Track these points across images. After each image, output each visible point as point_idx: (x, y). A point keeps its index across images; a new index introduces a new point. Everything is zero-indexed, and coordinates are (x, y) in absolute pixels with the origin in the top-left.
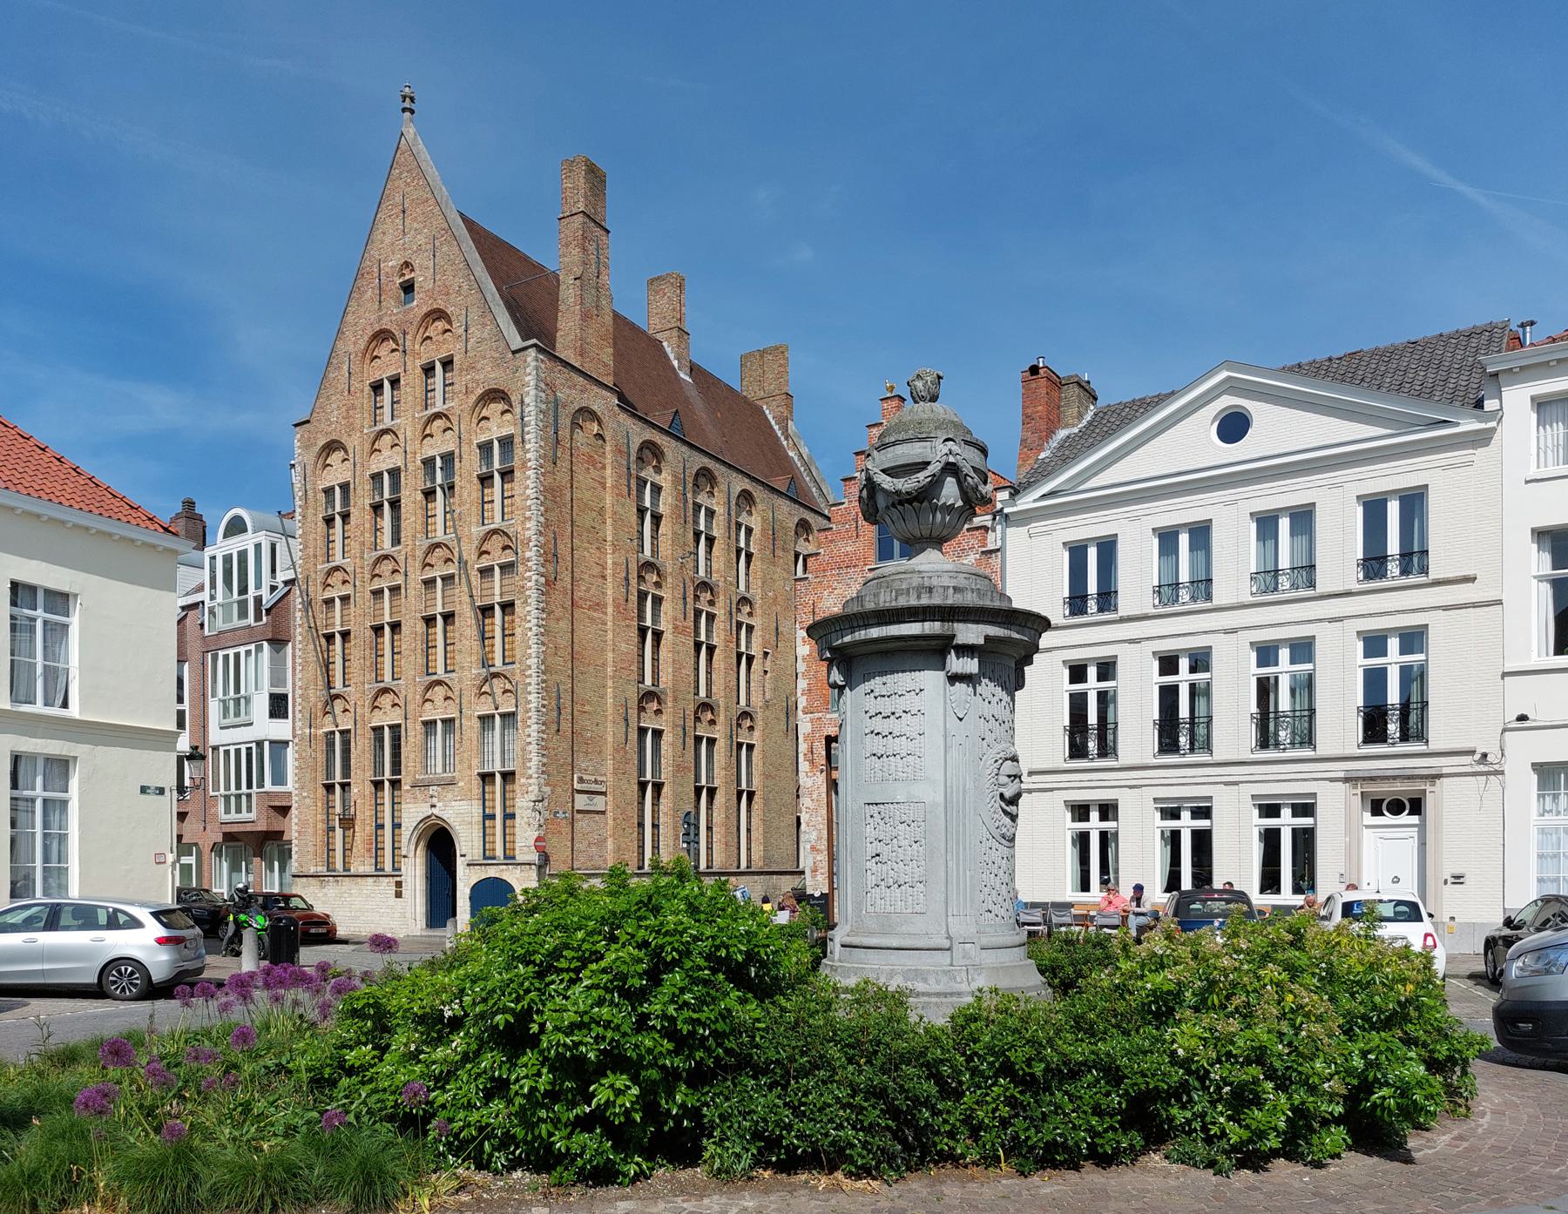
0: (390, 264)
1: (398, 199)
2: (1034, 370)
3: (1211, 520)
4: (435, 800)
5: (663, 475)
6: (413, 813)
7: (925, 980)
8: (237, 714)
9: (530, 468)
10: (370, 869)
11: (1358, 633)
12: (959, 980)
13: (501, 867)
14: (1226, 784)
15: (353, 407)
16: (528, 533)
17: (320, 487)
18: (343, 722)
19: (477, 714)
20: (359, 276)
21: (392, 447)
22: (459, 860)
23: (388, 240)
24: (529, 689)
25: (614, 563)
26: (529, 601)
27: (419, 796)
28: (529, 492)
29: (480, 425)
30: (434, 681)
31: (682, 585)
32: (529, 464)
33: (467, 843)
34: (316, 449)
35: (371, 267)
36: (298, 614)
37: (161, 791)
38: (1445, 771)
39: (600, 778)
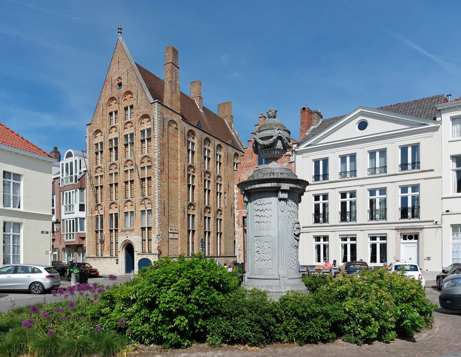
0: (115, 78)
1: (117, 58)
2: (304, 109)
3: (356, 153)
4: (128, 235)
5: (195, 140)
6: (122, 239)
7: (272, 288)
8: (70, 210)
9: (156, 138)
10: (109, 256)
11: (399, 186)
12: (282, 288)
13: (147, 255)
14: (361, 230)
15: (104, 120)
16: (155, 157)
17: (94, 143)
18: (101, 212)
19: (140, 210)
20: (106, 81)
21: (115, 131)
22: (135, 253)
23: (114, 71)
24: (156, 202)
25: (181, 166)
26: (156, 177)
27: (123, 234)
28: (155, 145)
29: (141, 125)
30: (128, 200)
31: (200, 172)
32: (156, 136)
33: (137, 248)
34: (93, 132)
35: (109, 78)
36: (88, 181)
37: (47, 233)
38: (425, 227)
39: (176, 229)
